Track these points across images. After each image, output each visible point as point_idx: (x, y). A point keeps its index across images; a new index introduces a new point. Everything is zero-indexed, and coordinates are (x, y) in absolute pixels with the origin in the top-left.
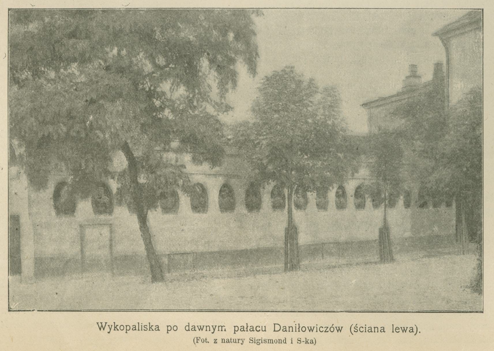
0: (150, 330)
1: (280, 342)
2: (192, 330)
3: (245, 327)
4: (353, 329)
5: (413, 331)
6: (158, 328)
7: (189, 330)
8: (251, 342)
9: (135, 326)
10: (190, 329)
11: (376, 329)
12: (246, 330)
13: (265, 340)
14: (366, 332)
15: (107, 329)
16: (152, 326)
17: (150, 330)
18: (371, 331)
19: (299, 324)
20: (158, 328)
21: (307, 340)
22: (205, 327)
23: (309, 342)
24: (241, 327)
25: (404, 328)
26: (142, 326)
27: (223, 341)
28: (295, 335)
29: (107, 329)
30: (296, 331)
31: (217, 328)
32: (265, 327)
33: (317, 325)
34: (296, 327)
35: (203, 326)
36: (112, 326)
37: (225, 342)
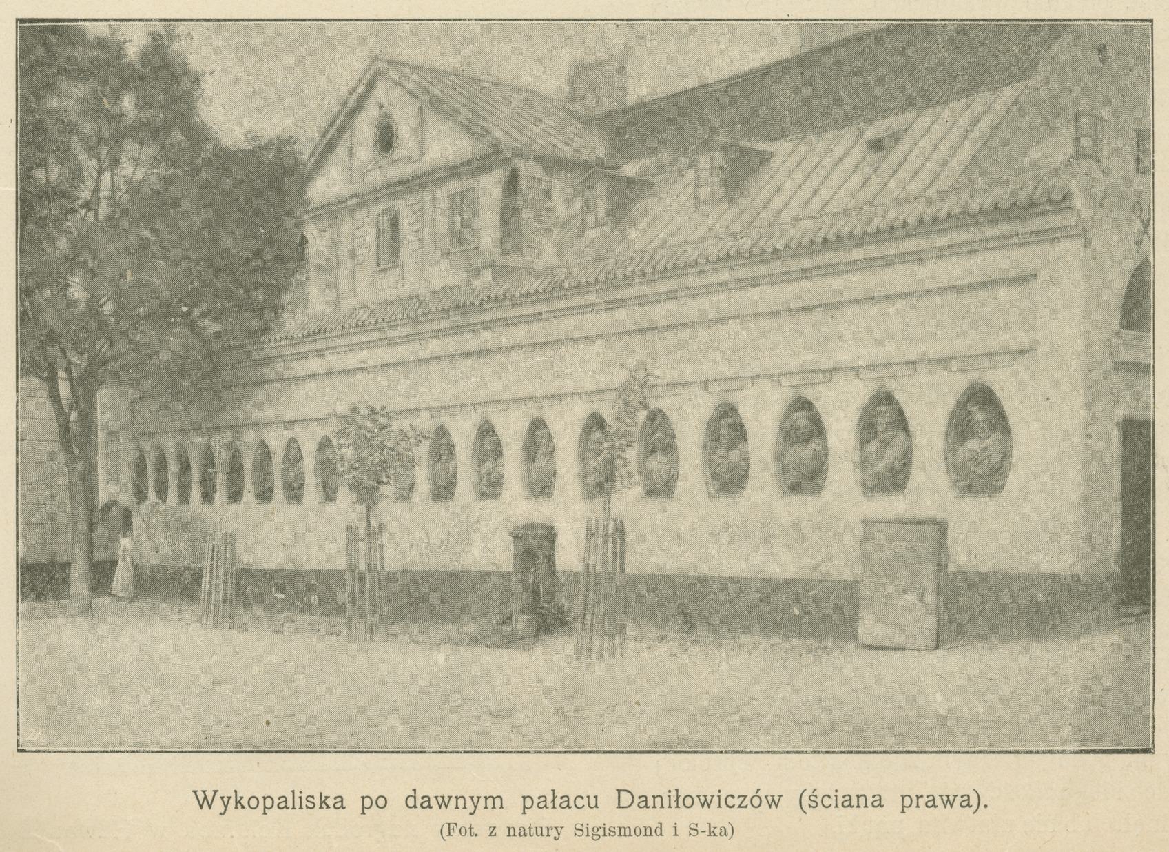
0: (321, 807)
1: (648, 833)
2: (540, 808)
3: (550, 798)
4: (805, 801)
5: (969, 805)
6: (340, 803)
7: (415, 806)
8: (579, 833)
9: (646, 797)
10: (418, 805)
11: (658, 800)
12: (675, 804)
13: (612, 829)
14: (837, 806)
15: (218, 805)
16: (327, 797)
17: (321, 807)
18: (545, 806)
19: (677, 790)
20: (340, 803)
21: (712, 829)
22: (453, 801)
23: (717, 831)
24: (279, 798)
25: (705, 796)
26: (301, 798)
27: (512, 833)
28: (684, 817)
29: (218, 805)
30: (670, 807)
31: (482, 801)
32: (596, 797)
33: (719, 791)
34: (669, 796)
35: (450, 797)
36: (229, 798)
37: (517, 834)
